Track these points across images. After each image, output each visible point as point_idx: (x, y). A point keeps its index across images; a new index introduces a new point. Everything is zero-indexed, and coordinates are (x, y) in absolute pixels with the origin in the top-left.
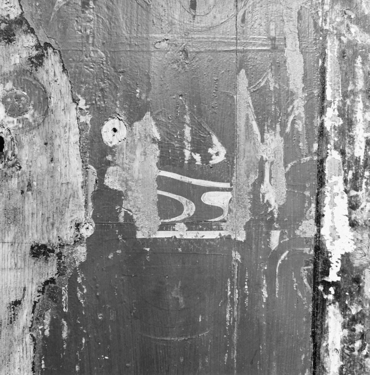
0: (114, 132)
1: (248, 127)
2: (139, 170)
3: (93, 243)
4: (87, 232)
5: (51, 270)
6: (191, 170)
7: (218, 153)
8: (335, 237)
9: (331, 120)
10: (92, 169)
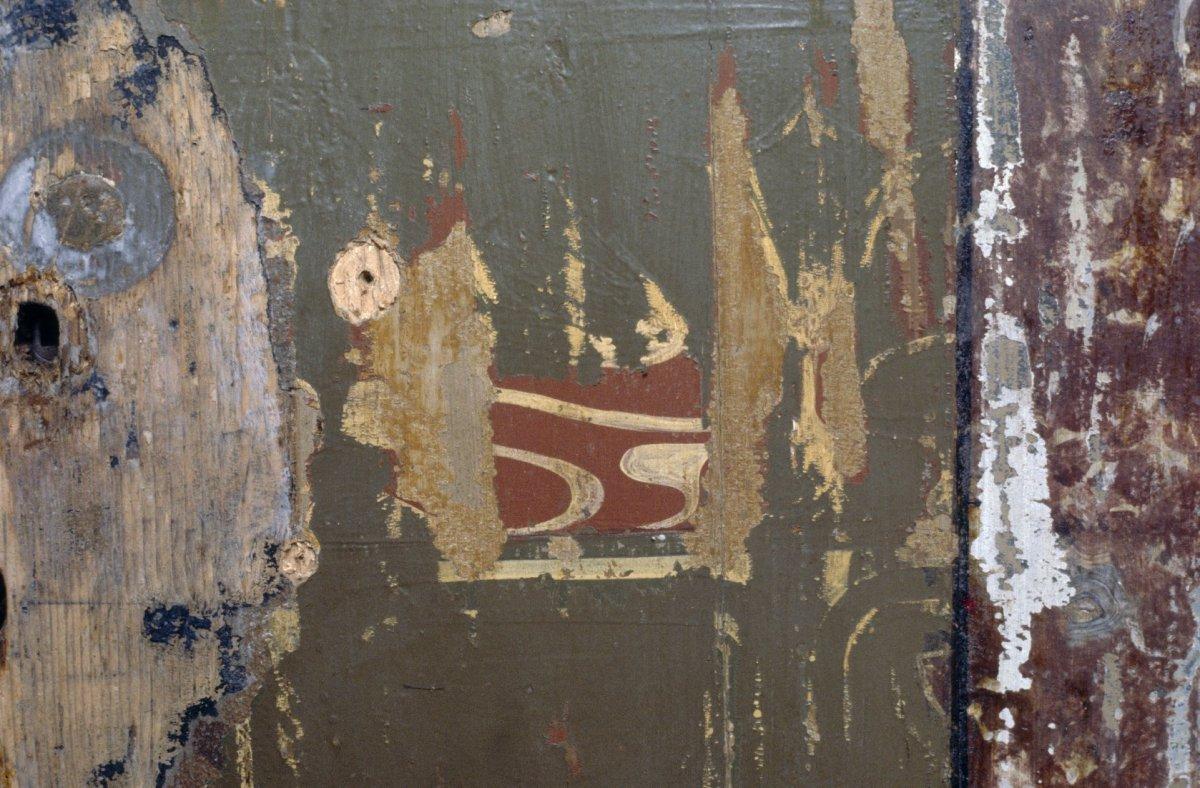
0: (363, 282)
3: (314, 598)
7: (665, 333)
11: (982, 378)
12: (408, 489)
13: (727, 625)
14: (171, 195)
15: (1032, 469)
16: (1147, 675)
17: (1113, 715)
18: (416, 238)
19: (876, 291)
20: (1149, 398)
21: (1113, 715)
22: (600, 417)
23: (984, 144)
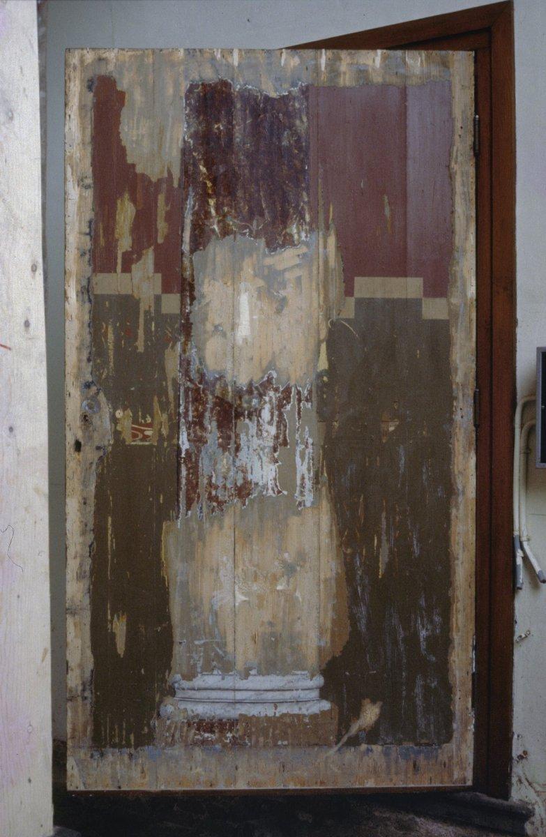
0: (119, 414)
1: (157, 412)
2: (126, 425)
3: (113, 445)
4: (112, 442)
5: (101, 453)
6: (141, 424)
7: (149, 420)
8: (183, 444)
9: (182, 409)
10: (113, 425)
11: (162, 539)
12: (123, 435)
13: (155, 449)
14: (100, 404)
15: (185, 435)
16: (197, 456)
17: (194, 460)
18: (124, 409)
19: (170, 419)
20: (197, 427)
21: (194, 460)
22: (142, 428)
23: (181, 402)
